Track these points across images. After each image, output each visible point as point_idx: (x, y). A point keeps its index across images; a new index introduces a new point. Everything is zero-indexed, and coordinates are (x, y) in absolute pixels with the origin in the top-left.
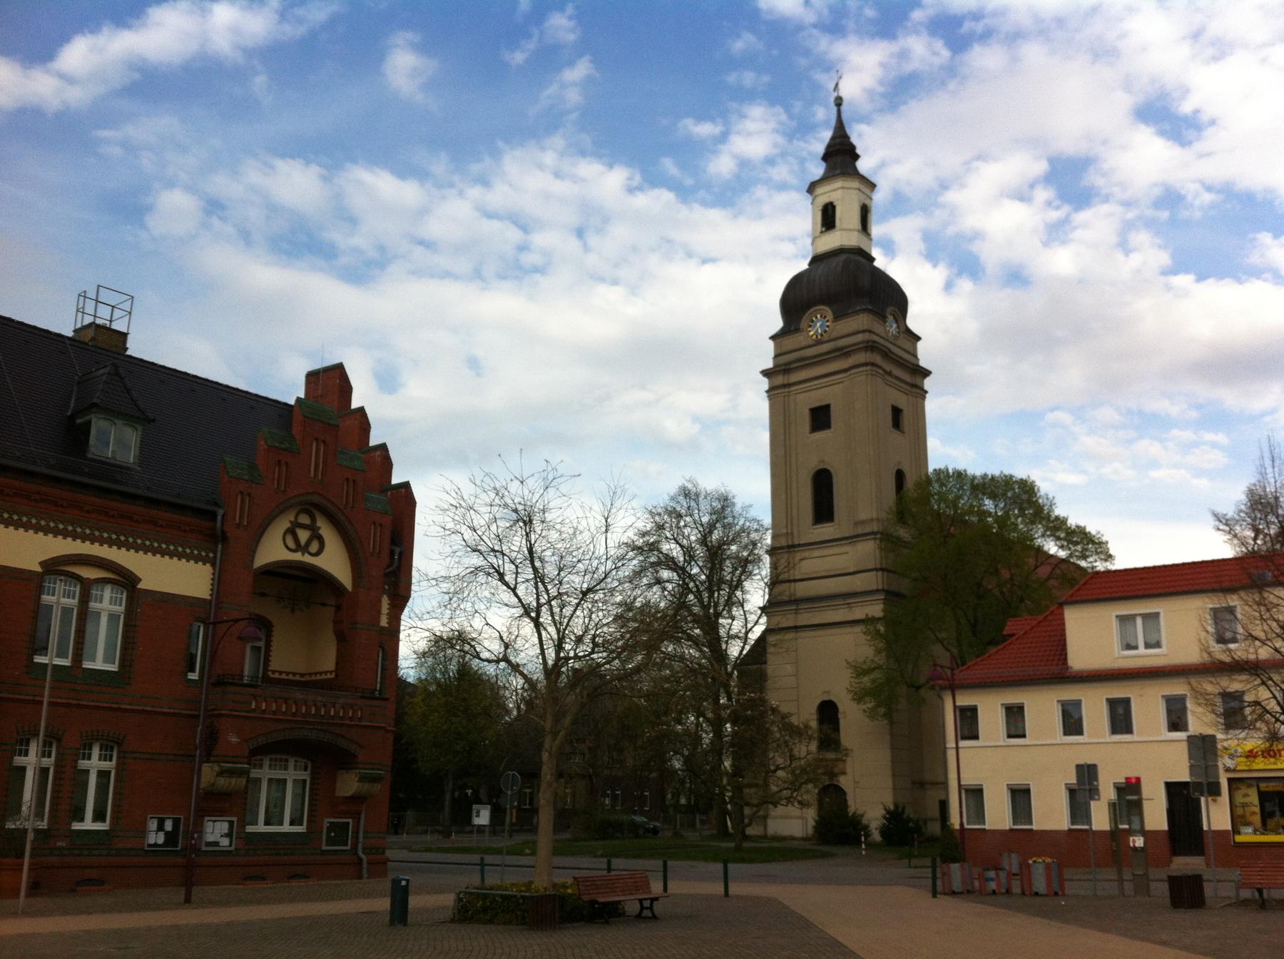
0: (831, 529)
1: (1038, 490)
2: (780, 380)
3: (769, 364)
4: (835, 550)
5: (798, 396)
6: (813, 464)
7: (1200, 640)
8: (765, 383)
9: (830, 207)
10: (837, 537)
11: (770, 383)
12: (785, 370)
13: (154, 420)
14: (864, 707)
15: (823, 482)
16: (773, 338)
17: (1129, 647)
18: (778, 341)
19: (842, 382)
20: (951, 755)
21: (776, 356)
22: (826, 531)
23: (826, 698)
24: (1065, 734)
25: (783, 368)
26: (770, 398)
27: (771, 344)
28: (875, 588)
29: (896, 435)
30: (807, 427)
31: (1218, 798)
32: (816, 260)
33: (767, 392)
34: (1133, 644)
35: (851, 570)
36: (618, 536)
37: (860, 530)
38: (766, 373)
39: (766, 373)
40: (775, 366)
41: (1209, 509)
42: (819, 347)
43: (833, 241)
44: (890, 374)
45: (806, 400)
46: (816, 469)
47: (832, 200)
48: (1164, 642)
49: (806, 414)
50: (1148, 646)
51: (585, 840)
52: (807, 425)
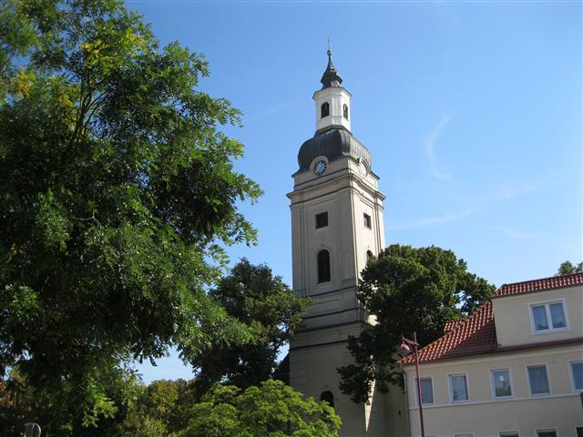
6: (316, 247)
8: (289, 202)
14: (350, 396)
15: (323, 258)
17: (540, 327)
20: (415, 417)
22: (326, 286)
23: (326, 390)
24: (534, 392)
29: (367, 229)
30: (314, 225)
32: (319, 133)
34: (544, 325)
36: (200, 59)
37: (346, 285)
38: (289, 196)
39: (289, 196)
43: (325, 123)
44: (362, 195)
45: (314, 209)
48: (568, 323)
49: (314, 218)
50: (555, 326)
51: (360, 183)
52: (314, 224)
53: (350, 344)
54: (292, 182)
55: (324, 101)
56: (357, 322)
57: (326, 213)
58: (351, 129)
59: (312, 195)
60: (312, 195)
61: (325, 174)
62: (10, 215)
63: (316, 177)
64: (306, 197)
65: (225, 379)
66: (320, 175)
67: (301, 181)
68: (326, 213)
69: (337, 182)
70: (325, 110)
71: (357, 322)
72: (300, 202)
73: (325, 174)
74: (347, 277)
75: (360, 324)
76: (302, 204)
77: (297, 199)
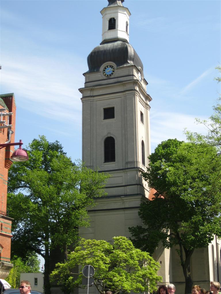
0: (114, 165)
1: (199, 137)
2: (88, 93)
3: (83, 86)
4: (116, 175)
5: (97, 102)
6: (105, 134)
7: (135, 76)
8: (81, 95)
9: (113, 20)
10: (116, 169)
11: (83, 95)
12: (92, 89)
13: (2, 230)
16: (84, 74)
18: (88, 75)
19: (121, 97)
21: (86, 83)
22: (111, 165)
25: (91, 88)
26: (82, 101)
27: (84, 78)
28: (137, 193)
31: (39, 139)
33: (81, 99)
35: (124, 184)
38: (81, 90)
39: (81, 90)
40: (86, 87)
41: (218, 83)
42: (109, 80)
46: (106, 137)
47: (114, 17)
53: (141, 210)
54: (83, 79)
55: (112, 16)
56: (137, 194)
57: (79, 89)
58: (129, 42)
59: (101, 92)
60: (101, 92)
61: (112, 76)
62: (33, 246)
63: (105, 78)
64: (95, 93)
65: (50, 282)
66: (109, 77)
67: (90, 80)
68: (79, 89)
69: (124, 85)
70: (112, 24)
71: (137, 194)
72: (94, 96)
73: (112, 76)
74: (130, 160)
75: (140, 197)
76: (92, 98)
77: (88, 93)
